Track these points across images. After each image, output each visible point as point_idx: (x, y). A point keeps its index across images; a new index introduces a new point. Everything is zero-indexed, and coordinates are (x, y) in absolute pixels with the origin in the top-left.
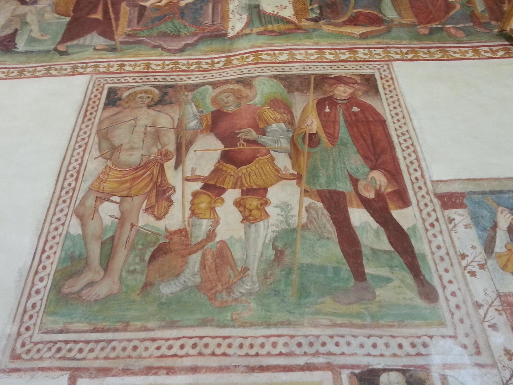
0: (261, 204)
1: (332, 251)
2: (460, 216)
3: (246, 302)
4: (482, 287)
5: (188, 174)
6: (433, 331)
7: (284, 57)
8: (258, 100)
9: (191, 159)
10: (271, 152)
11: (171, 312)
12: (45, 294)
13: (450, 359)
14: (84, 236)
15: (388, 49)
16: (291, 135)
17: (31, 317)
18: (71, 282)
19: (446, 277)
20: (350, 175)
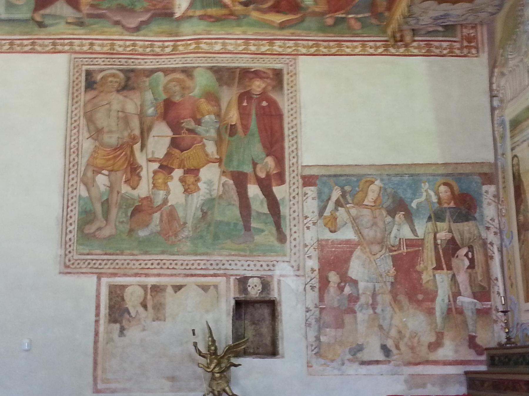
0: (196, 181)
1: (233, 213)
2: (311, 191)
3: (185, 242)
4: (310, 236)
5: (150, 156)
6: (278, 259)
7: (218, 47)
8: (196, 92)
9: (151, 142)
10: (204, 140)
11: (146, 246)
12: (75, 232)
13: (284, 273)
14: (90, 198)
15: (299, 42)
16: (218, 126)
17: (70, 246)
18: (87, 227)
19: (294, 229)
20: (253, 160)
